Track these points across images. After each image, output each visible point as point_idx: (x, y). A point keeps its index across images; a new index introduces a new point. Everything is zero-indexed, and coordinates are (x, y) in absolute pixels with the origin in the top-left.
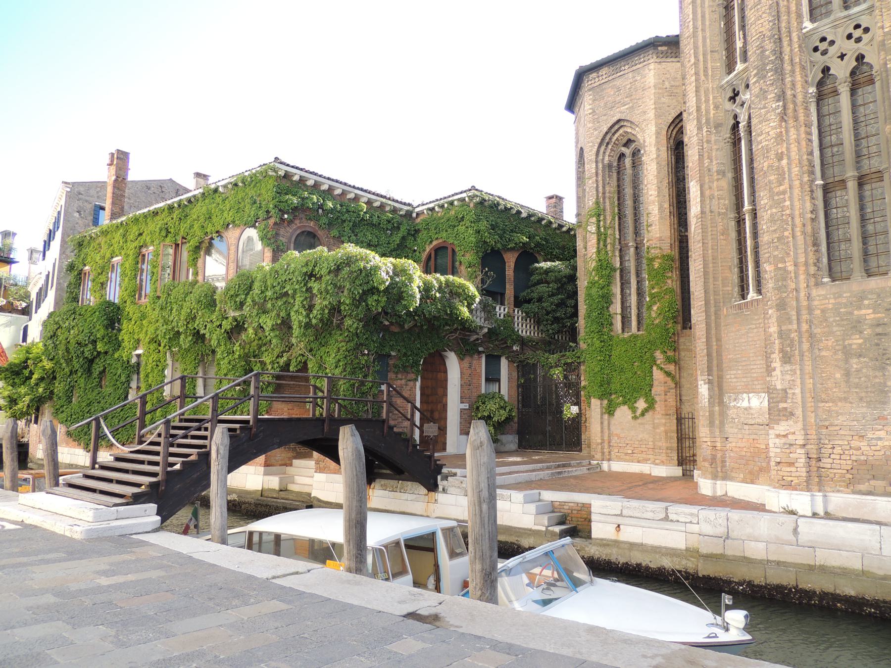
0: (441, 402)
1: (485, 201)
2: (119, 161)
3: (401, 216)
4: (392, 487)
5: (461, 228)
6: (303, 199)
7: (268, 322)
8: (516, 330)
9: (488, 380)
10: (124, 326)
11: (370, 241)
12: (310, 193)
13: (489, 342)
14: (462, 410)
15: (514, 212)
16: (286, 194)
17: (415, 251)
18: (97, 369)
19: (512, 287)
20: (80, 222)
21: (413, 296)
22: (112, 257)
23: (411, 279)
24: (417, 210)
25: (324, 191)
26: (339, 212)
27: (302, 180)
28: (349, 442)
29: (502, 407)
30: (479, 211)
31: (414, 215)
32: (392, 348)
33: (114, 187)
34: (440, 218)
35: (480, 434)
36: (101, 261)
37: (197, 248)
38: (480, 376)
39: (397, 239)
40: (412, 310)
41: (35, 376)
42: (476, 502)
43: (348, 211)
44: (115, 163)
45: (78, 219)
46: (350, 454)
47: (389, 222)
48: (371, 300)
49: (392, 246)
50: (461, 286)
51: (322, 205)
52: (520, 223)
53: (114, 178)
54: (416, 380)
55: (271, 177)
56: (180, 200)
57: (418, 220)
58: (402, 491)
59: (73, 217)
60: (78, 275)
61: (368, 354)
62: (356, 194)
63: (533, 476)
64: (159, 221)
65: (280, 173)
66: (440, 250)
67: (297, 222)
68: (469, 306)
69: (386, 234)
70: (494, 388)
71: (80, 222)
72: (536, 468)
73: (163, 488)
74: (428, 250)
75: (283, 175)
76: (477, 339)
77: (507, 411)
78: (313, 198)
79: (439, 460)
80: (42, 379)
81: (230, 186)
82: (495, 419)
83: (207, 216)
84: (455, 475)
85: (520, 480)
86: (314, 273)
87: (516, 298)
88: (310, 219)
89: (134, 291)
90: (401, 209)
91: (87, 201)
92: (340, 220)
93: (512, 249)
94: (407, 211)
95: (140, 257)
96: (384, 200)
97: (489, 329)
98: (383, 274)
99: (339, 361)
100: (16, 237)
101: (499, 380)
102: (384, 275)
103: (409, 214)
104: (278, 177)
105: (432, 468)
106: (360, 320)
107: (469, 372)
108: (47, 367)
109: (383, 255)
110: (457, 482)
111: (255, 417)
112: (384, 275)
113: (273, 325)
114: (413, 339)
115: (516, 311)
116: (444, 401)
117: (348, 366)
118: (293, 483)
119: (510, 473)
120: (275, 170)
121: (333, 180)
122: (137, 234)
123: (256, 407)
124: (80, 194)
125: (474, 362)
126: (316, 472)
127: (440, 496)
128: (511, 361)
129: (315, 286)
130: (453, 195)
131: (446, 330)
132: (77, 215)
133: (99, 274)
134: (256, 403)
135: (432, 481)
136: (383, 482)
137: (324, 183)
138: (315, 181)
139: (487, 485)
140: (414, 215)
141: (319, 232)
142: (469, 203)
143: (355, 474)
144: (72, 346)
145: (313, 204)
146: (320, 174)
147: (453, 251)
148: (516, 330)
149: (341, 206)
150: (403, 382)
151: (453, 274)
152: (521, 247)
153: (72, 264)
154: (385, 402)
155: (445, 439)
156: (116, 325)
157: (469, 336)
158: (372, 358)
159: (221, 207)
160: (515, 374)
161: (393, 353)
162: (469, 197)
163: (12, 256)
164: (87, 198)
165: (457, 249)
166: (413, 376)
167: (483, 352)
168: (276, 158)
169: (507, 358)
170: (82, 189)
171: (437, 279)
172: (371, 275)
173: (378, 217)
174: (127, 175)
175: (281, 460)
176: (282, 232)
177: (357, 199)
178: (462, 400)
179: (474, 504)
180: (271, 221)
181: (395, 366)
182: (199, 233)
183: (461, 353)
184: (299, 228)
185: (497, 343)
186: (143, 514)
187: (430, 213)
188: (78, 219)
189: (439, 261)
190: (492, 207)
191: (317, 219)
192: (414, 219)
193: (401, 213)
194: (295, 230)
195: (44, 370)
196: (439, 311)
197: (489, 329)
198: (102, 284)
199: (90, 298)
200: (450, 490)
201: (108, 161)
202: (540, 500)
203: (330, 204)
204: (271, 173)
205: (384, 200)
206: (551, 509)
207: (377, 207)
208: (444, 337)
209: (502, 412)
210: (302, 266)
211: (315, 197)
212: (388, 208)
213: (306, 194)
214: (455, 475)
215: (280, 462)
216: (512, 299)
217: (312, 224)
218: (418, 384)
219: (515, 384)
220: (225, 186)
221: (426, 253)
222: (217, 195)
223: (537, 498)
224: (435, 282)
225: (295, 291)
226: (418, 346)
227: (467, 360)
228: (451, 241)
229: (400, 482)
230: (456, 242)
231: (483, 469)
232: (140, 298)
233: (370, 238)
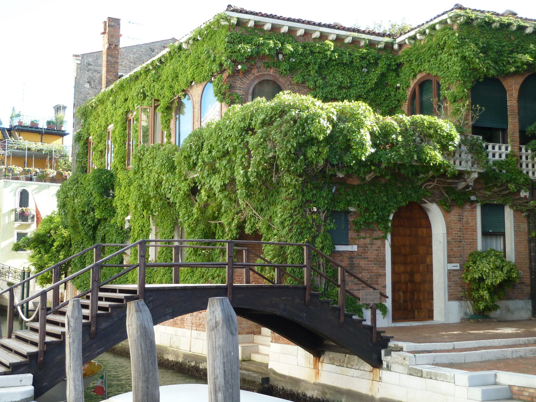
0: (424, 262)
1: (472, 20)
2: (110, 28)
3: (380, 49)
4: (340, 361)
5: (444, 56)
6: (258, 46)
7: (217, 182)
8: (525, 172)
9: (485, 234)
10: (117, 193)
11: (342, 83)
12: (267, 39)
13: (485, 189)
14: (450, 272)
15: (515, 28)
16: (240, 43)
17: (398, 88)
18: (100, 233)
19: (516, 120)
20: (91, 92)
21: (362, 145)
22: (108, 125)
23: (360, 125)
24: (399, 40)
25: (284, 33)
26: (301, 55)
27: (258, 26)
28: (133, 318)
29: (497, 268)
30: (465, 33)
31: (396, 47)
32: (349, 204)
33: (108, 55)
34: (423, 47)
35: (216, 313)
36: (99, 129)
37: (168, 108)
38: (475, 231)
39: (374, 77)
40: (363, 159)
41: (56, 244)
42: (212, 389)
43: (312, 53)
44: (107, 31)
45: (89, 89)
46: (135, 331)
47: (364, 58)
48: (311, 152)
49: (370, 85)
50: (431, 126)
51: (280, 49)
52: (523, 41)
53: (107, 46)
54: (385, 238)
55: (223, 27)
56: (152, 62)
57: (400, 53)
58: (349, 366)
59: (84, 87)
60: (84, 144)
61: (318, 212)
62: (321, 33)
63: (508, 352)
64: (137, 88)
65: (232, 21)
66: (423, 85)
67: (255, 71)
68: (444, 148)
69: (361, 73)
70: (496, 244)
71: (91, 92)
72: (518, 343)
73: (41, 359)
74: (412, 85)
75: (235, 22)
76: (467, 187)
77: (505, 271)
78: (269, 44)
79: (384, 332)
80: (62, 246)
81: (191, 42)
82: (488, 282)
83: (174, 75)
84: (401, 349)
85: (488, 357)
86: (251, 127)
87: (522, 133)
88: (268, 67)
89: (123, 157)
90: (379, 42)
91: (96, 71)
92: (303, 64)
93: (515, 73)
94: (387, 44)
95: (126, 122)
96: (356, 34)
97: (479, 173)
98: (322, 121)
99: (285, 220)
100: (67, 109)
101: (503, 234)
102: (325, 123)
103: (389, 47)
104: (231, 26)
105: (374, 340)
106: (300, 176)
107: (459, 226)
108: (65, 235)
109: (325, 100)
110: (400, 358)
111: (142, 285)
112: (325, 123)
113: (221, 186)
114: (377, 191)
115: (523, 150)
116: (428, 260)
117: (295, 226)
118: (257, 352)
119: (479, 348)
120: (227, 19)
121: (294, 21)
122: (123, 100)
123: (142, 276)
124: (89, 64)
125: (466, 214)
126: (272, 342)
127: (384, 374)
128: (517, 211)
129: (252, 140)
130: (435, 18)
131: (421, 179)
132: (87, 85)
133: (99, 143)
134: (142, 272)
135: (375, 356)
136: (332, 355)
137: (315, 31)
138: (272, 24)
139: (222, 372)
140: (396, 47)
141: (281, 79)
142: (452, 25)
143: (140, 352)
144: (78, 213)
145: (270, 50)
146: (279, 15)
147: (438, 83)
148: (525, 172)
149: (304, 47)
150: (368, 241)
151: (422, 112)
152: (526, 71)
153: (79, 134)
154: (305, 267)
155: (432, 305)
156: (111, 191)
157: (457, 183)
158: (323, 216)
159: (184, 64)
160: (524, 226)
161: (352, 209)
162: (451, 18)
163: (63, 129)
164: (96, 68)
165: (441, 81)
166: (380, 234)
167: (477, 201)
168: (229, 6)
169: (511, 207)
170: (90, 60)
171: (400, 122)
172: (308, 125)
173: (350, 54)
174: (119, 41)
175: (248, 328)
176: (238, 84)
177: (323, 36)
178: (450, 259)
179: (211, 393)
180: (225, 75)
181: (356, 223)
182: (167, 93)
183: (445, 205)
184: (257, 77)
185: (495, 189)
186: (19, 384)
187: (413, 42)
188: (89, 89)
189: (425, 98)
190: (483, 26)
191: (276, 65)
192: (397, 51)
193: (379, 46)
194: (253, 80)
195: (63, 238)
196: (402, 158)
197: (479, 173)
198: (101, 152)
199: (94, 165)
200: (394, 367)
201: (103, 31)
202: (496, 384)
203: (290, 47)
204: (223, 23)
205: (356, 34)
206: (509, 395)
207: (348, 43)
208: (421, 186)
209: (498, 273)
210: (240, 122)
211: (271, 42)
212: (362, 43)
213: (261, 40)
214: (401, 349)
215: (247, 330)
216: (517, 135)
217: (272, 72)
218: (388, 243)
219: (525, 238)
220: (187, 42)
221: (410, 89)
222: (182, 52)
223: (492, 380)
224: (395, 124)
225: (235, 148)
226: (385, 199)
227: (455, 213)
228: (434, 73)
229: (347, 355)
230: (439, 74)
231: (218, 353)
232: (129, 165)
233: (341, 79)
